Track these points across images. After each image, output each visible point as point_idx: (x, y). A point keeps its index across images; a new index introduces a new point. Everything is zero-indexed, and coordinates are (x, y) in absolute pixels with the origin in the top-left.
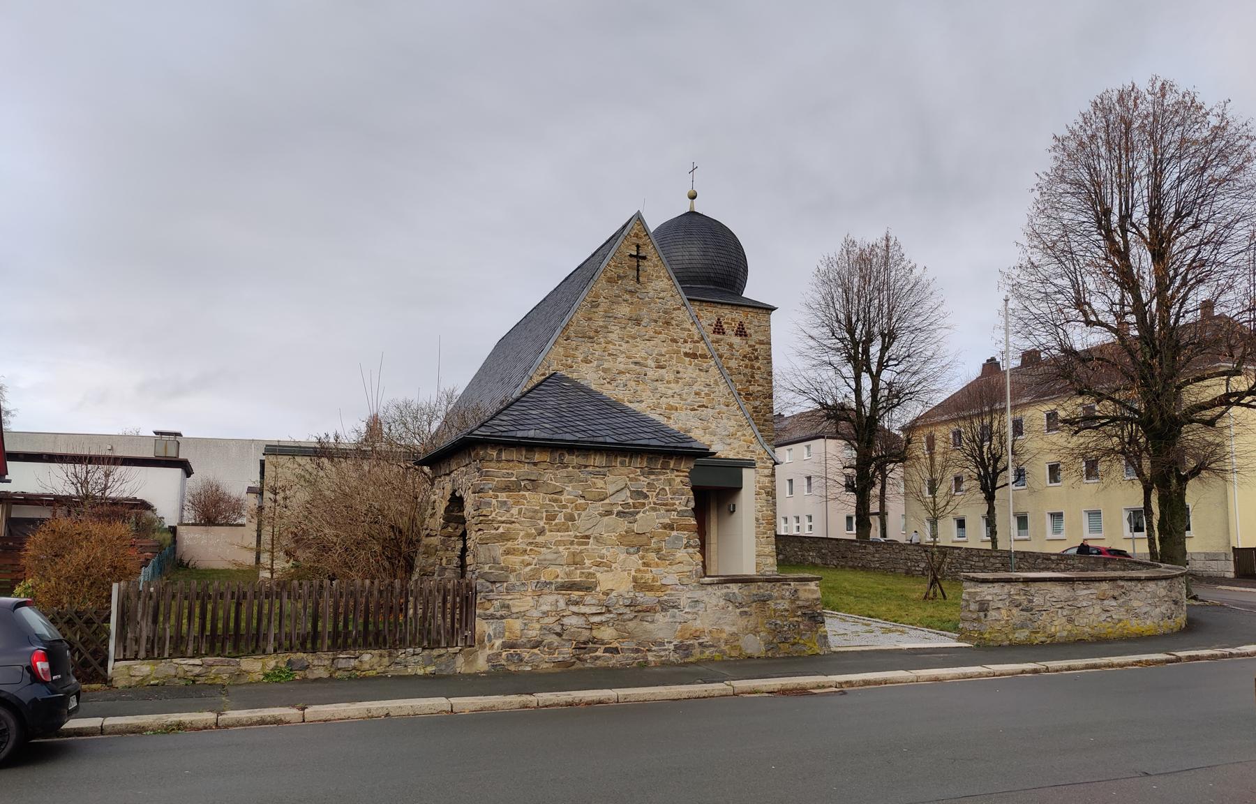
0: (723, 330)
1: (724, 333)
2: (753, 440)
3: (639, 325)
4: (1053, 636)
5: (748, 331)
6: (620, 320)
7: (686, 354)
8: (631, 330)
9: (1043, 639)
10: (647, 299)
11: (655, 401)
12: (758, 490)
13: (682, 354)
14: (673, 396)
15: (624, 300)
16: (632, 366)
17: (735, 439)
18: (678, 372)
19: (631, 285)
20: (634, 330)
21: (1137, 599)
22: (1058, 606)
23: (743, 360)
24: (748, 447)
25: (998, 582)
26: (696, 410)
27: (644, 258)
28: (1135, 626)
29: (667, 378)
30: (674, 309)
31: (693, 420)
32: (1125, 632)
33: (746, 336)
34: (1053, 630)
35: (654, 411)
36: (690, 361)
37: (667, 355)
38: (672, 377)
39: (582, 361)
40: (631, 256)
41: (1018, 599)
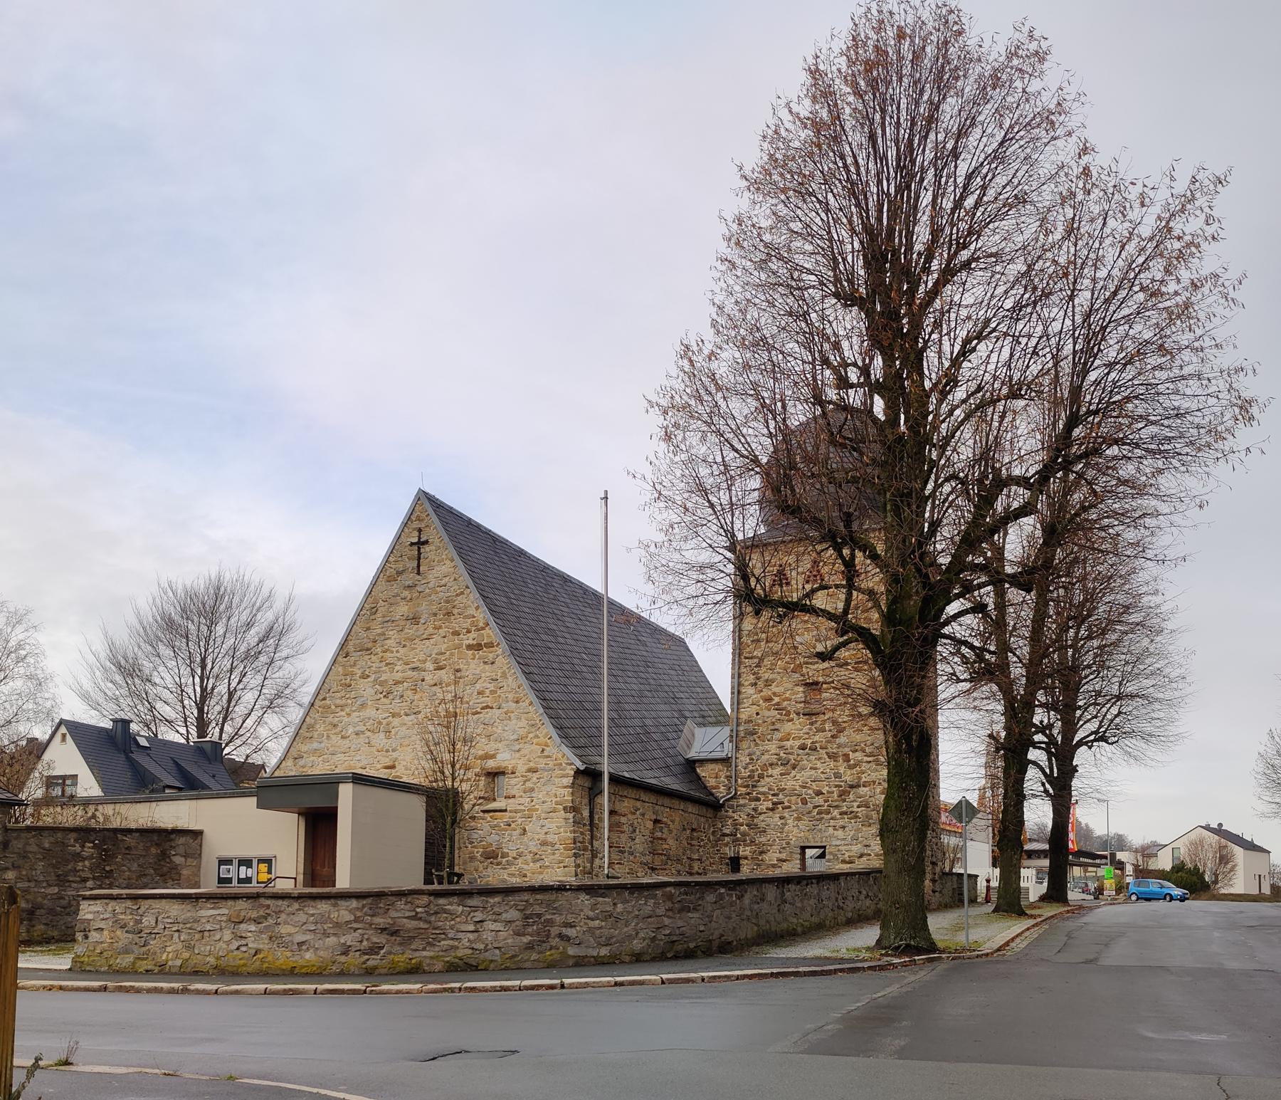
7: (469, 647)
16: (410, 672)
18: (458, 671)
19: (410, 578)
20: (410, 631)
21: (288, 924)
22: (174, 929)
24: (543, 750)
26: (480, 713)
27: (426, 542)
28: (283, 958)
30: (457, 595)
32: (266, 965)
34: (164, 957)
36: (473, 654)
40: (412, 544)
41: (123, 919)
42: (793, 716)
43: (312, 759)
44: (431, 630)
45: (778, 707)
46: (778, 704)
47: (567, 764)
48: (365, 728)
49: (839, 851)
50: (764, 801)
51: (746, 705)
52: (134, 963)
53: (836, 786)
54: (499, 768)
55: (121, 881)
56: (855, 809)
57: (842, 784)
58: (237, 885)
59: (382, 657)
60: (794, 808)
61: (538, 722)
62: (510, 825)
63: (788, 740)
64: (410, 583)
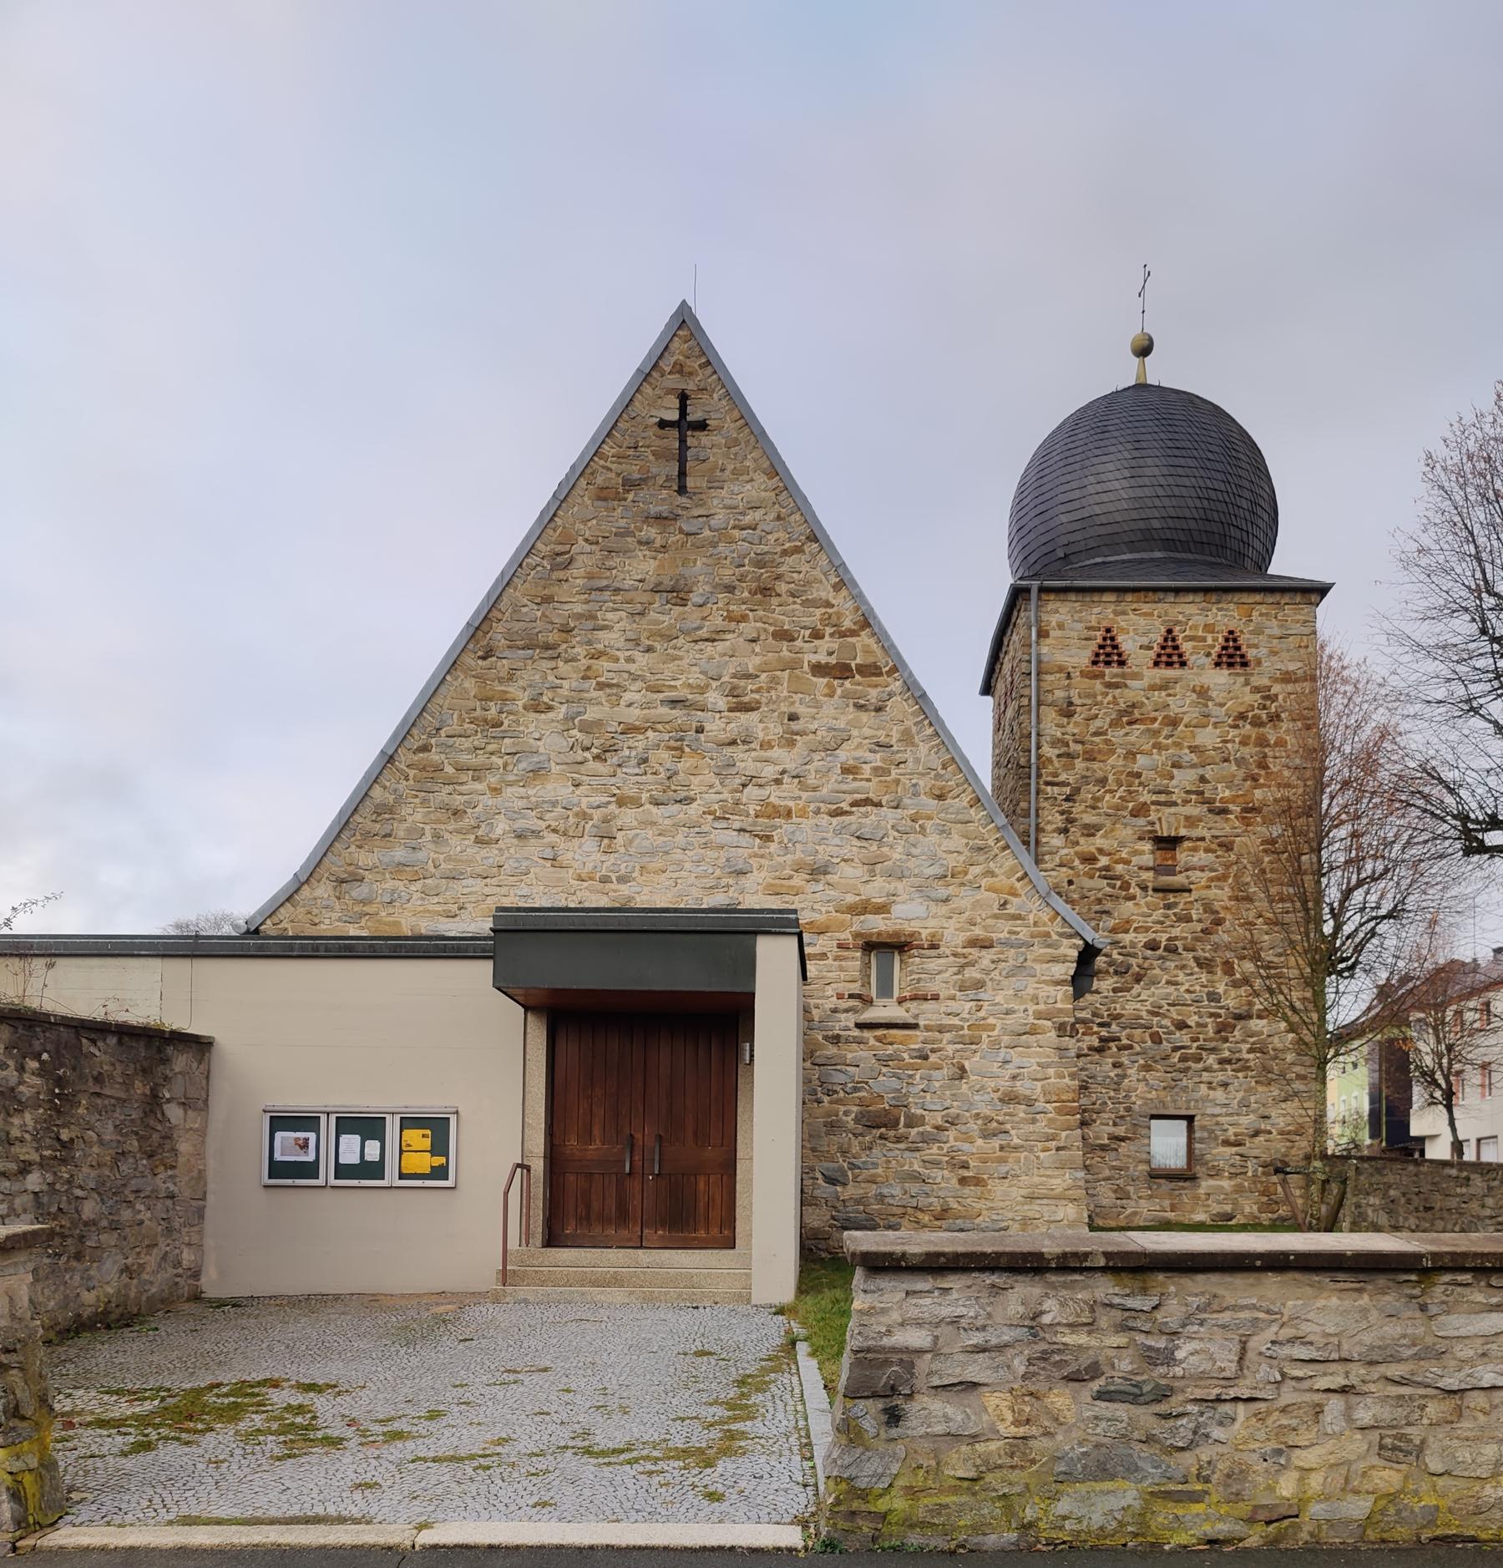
0: (1180, 656)
1: (1183, 664)
2: (1018, 885)
3: (683, 602)
4: (1284, 1516)
5: (1251, 654)
6: (629, 596)
7: (818, 669)
8: (661, 617)
9: (1222, 1529)
10: (707, 533)
11: (726, 795)
12: (1031, 1020)
13: (806, 667)
14: (778, 782)
15: (640, 543)
16: (664, 710)
17: (963, 884)
18: (793, 717)
19: (661, 499)
20: (664, 616)
22: (1323, 1383)
23: (1236, 727)
24: (1004, 905)
25: (965, 1270)
27: (702, 426)
29: (761, 735)
30: (785, 553)
31: (837, 841)
33: (1245, 664)
34: (1287, 1487)
35: (724, 824)
37: (764, 676)
38: (775, 730)
39: (525, 708)
40: (663, 424)
42: (1134, 890)
43: (390, 884)
44: (718, 621)
45: (1107, 874)
46: (1107, 868)
47: (1061, 935)
48: (543, 825)
49: (1217, 1124)
50: (1083, 1034)
51: (1049, 866)
52: (1142, 1517)
53: (1212, 1015)
54: (896, 934)
55: (85, 1170)
56: (1246, 1056)
57: (1222, 1011)
58: (333, 1181)
59: (589, 668)
60: (1137, 1048)
61: (991, 842)
62: (926, 1058)
63: (1127, 931)
64: (663, 509)
